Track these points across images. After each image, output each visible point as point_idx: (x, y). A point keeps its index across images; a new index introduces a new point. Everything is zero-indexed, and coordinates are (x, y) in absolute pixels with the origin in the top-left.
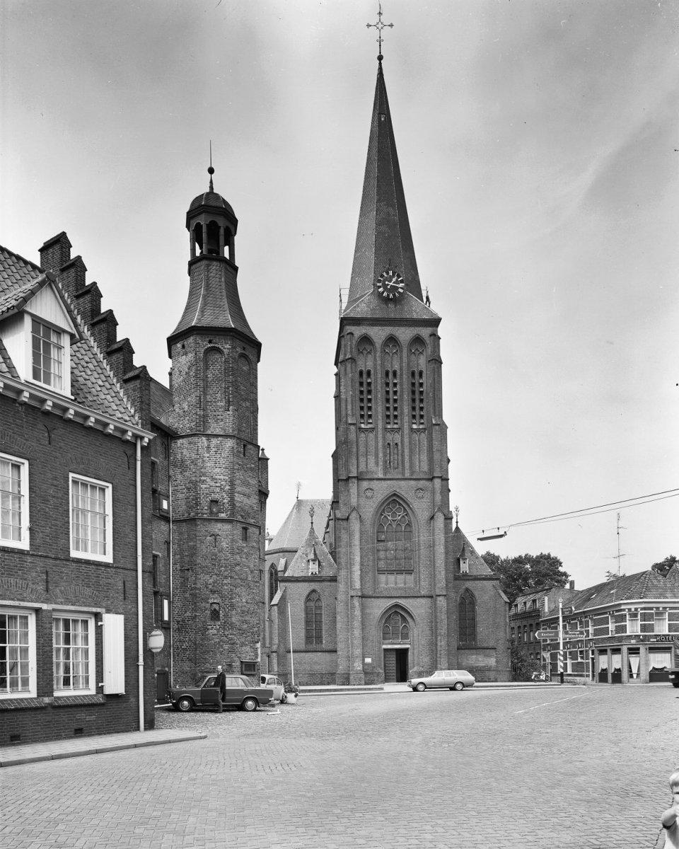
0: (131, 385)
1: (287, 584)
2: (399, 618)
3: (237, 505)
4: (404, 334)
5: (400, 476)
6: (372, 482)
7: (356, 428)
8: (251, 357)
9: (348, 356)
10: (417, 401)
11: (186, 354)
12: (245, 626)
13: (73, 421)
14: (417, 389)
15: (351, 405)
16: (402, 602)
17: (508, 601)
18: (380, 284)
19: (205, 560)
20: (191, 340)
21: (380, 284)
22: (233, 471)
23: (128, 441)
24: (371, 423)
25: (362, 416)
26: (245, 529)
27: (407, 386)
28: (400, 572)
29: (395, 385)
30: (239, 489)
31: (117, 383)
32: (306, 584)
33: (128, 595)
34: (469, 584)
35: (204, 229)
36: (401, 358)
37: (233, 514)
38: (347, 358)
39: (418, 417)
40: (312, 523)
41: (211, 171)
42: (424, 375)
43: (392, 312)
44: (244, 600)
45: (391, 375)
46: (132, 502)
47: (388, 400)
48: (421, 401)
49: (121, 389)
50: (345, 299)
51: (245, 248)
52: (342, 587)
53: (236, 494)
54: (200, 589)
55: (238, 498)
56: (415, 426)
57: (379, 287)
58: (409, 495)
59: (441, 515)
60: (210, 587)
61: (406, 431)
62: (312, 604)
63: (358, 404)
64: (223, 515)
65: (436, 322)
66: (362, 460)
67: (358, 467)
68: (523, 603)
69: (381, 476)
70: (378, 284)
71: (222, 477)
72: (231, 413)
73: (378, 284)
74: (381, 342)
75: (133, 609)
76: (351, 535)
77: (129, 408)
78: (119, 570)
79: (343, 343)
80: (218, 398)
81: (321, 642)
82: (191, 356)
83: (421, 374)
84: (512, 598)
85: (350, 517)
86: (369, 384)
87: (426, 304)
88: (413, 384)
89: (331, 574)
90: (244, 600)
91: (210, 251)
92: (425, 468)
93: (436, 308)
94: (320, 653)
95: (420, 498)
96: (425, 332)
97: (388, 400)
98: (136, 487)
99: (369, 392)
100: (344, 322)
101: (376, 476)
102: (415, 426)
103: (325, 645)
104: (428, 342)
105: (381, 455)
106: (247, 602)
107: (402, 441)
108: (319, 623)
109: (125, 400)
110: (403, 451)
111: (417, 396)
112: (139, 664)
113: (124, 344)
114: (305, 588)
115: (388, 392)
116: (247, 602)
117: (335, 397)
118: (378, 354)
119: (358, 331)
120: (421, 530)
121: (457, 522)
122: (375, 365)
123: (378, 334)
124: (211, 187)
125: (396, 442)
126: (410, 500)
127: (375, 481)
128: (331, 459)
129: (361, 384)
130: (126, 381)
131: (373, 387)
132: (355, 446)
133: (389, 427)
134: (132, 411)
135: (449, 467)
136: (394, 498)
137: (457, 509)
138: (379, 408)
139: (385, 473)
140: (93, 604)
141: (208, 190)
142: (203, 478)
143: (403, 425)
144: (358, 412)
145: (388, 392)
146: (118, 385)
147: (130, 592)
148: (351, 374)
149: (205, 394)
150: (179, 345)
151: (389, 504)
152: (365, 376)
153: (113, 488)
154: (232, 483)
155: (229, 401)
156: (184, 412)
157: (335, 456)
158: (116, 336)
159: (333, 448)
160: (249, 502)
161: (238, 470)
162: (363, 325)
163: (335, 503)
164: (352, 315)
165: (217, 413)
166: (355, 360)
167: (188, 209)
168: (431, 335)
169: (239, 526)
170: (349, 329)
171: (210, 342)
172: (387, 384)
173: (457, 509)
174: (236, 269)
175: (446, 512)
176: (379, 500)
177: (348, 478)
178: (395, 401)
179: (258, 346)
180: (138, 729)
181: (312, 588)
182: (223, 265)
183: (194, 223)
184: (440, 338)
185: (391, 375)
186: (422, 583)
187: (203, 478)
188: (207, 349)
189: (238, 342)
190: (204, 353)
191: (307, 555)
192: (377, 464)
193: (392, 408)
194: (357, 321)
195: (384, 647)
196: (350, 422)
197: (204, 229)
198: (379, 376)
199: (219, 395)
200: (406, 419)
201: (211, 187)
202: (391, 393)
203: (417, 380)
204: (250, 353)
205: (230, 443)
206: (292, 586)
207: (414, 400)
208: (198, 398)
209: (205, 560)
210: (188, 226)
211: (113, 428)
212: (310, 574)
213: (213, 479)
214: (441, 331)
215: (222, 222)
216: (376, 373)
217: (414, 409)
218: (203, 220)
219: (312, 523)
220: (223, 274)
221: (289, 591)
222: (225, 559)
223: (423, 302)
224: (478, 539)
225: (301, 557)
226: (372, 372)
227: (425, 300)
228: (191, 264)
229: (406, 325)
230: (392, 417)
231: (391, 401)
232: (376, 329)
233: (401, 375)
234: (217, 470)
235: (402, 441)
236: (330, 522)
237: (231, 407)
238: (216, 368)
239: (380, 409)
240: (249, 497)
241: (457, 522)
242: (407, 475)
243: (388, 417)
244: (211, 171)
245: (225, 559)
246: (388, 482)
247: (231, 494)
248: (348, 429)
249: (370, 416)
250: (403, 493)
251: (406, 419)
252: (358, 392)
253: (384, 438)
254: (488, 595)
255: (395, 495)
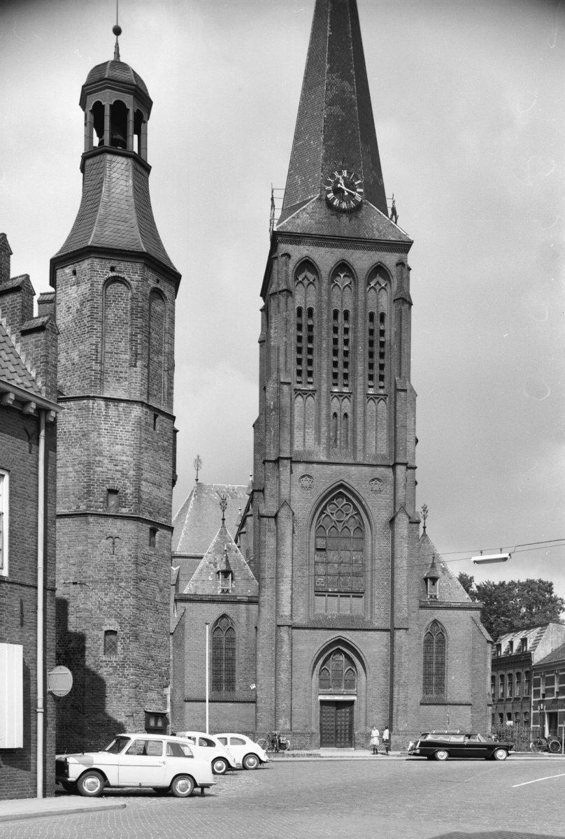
0: (31, 339)
1: (187, 605)
2: (342, 658)
3: (144, 497)
4: (362, 260)
5: (351, 461)
6: (310, 466)
7: (290, 389)
8: (167, 294)
9: (283, 287)
10: (376, 356)
11: (78, 283)
12: (151, 664)
13: (13, 408)
14: (377, 339)
15: (284, 356)
16: (347, 635)
17: (491, 640)
18: (330, 188)
19: (99, 571)
20: (85, 265)
21: (330, 188)
22: (140, 449)
23: (29, 416)
24: (311, 383)
25: (299, 373)
26: (153, 532)
27: (363, 336)
28: (346, 594)
29: (346, 331)
30: (146, 475)
31: (12, 334)
32: (214, 606)
33: (25, 621)
34: (440, 615)
35: (107, 111)
36: (356, 294)
37: (138, 510)
38: (280, 289)
39: (376, 378)
40: (223, 519)
41: (117, 31)
42: (387, 319)
43: (345, 226)
44: (150, 629)
45: (341, 316)
46: (33, 496)
47: (335, 353)
48: (382, 355)
49: (17, 342)
50: (279, 204)
51: (161, 135)
52: (267, 613)
53: (143, 482)
54: (90, 611)
55: (145, 487)
56: (371, 391)
57: (329, 192)
58: (362, 489)
59: (405, 517)
60: (105, 608)
61: (360, 397)
62: (223, 635)
63: (294, 356)
64: (124, 511)
65: (404, 246)
66: (298, 434)
67: (292, 445)
68: (510, 642)
69: (324, 459)
70: (327, 188)
71: (124, 458)
72: (138, 369)
73: (327, 188)
74: (328, 269)
75: (31, 638)
76: (279, 540)
77: (29, 370)
78: (15, 586)
79: (275, 267)
80: (120, 346)
81: (233, 689)
82: (85, 287)
83: (382, 316)
84: (496, 634)
85: (279, 514)
86: (310, 328)
87: (391, 219)
88: (371, 332)
89: (249, 592)
90: (150, 629)
91: (114, 142)
92: (384, 449)
93: (407, 225)
94: (231, 704)
95: (375, 492)
96: (390, 259)
97: (335, 353)
98: (37, 474)
99: (310, 339)
100: (276, 238)
101: (316, 459)
102: (371, 391)
103: (239, 693)
104: (394, 273)
105: (324, 429)
106: (153, 631)
107: (354, 412)
108: (231, 661)
109: (23, 358)
110: (355, 425)
111: (377, 349)
112: (38, 710)
113: (23, 282)
114: (215, 610)
115: (336, 341)
116: (153, 631)
117: (260, 342)
118: (325, 286)
119: (298, 252)
120: (377, 536)
121: (424, 528)
122: (320, 301)
123: (325, 258)
124: (117, 54)
125: (345, 411)
126: (363, 494)
127: (315, 465)
128: (252, 429)
129: (299, 327)
130: (25, 333)
131: (315, 332)
132: (288, 414)
133: (336, 390)
134: (33, 374)
135: (417, 450)
136: (341, 490)
137: (425, 509)
138: (323, 363)
139: (328, 455)
140: (475, 690)
141: (111, 57)
142: (98, 458)
143: (356, 389)
144: (293, 367)
145: (336, 341)
146: (13, 338)
147: (28, 615)
148: (286, 312)
149: (103, 342)
150: (68, 270)
151: (332, 499)
152: (304, 315)
153: (11, 477)
154: (139, 468)
155: (137, 354)
156: (73, 364)
157: (256, 426)
158: (9, 270)
159: (255, 414)
160: (159, 494)
161: (146, 448)
162: (305, 243)
163: (257, 491)
164: (289, 229)
165: (120, 369)
166: (291, 293)
167: (83, 81)
168: (397, 265)
169: (147, 527)
170: (284, 247)
171: (112, 269)
172: (336, 330)
173: (425, 509)
174: (148, 169)
175: (410, 513)
176: (321, 491)
177: (277, 461)
178: (346, 353)
179: (174, 278)
180: (34, 795)
181: (221, 613)
182: (130, 161)
183: (91, 101)
184: (409, 269)
185: (341, 316)
186: (376, 611)
187: (98, 458)
188: (107, 279)
189: (149, 274)
190: (106, 281)
191: (215, 565)
192: (318, 440)
193: (340, 364)
194: (295, 238)
195: (321, 698)
196: (282, 380)
197: (107, 111)
198: (325, 317)
199: (122, 344)
200: (360, 380)
201: (117, 54)
202: (341, 342)
203: (377, 326)
204: (165, 287)
205: (137, 411)
206: (193, 609)
207: (371, 355)
208: (94, 347)
209: (99, 571)
210: (83, 104)
211: (13, 398)
212: (219, 592)
213: (111, 459)
214: (412, 258)
215: (129, 101)
216: (320, 313)
217: (371, 366)
218: (107, 98)
219: (223, 519)
220: (131, 175)
221: (189, 615)
222: (125, 571)
223: (387, 216)
224: (475, 562)
225: (207, 567)
226: (315, 311)
227: (390, 212)
228: (85, 157)
229: (364, 248)
230: (340, 376)
231: (341, 354)
232: (322, 250)
233: (356, 318)
234: (119, 448)
235: (354, 412)
236: (249, 519)
237: (139, 363)
238: (121, 303)
239: (324, 364)
240: (159, 486)
241: (424, 528)
242: (360, 459)
243: (335, 376)
244: (117, 31)
245: (125, 571)
246: (334, 467)
247: (138, 479)
248: (279, 390)
249: (310, 374)
250: (353, 484)
251: (360, 380)
252: (294, 339)
253: (329, 405)
254: (463, 628)
255: (341, 486)
